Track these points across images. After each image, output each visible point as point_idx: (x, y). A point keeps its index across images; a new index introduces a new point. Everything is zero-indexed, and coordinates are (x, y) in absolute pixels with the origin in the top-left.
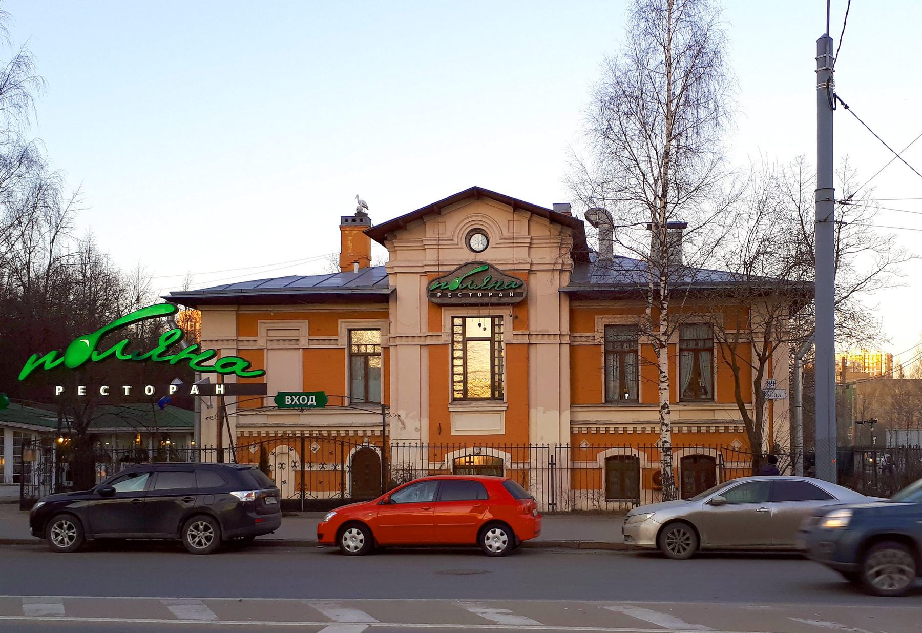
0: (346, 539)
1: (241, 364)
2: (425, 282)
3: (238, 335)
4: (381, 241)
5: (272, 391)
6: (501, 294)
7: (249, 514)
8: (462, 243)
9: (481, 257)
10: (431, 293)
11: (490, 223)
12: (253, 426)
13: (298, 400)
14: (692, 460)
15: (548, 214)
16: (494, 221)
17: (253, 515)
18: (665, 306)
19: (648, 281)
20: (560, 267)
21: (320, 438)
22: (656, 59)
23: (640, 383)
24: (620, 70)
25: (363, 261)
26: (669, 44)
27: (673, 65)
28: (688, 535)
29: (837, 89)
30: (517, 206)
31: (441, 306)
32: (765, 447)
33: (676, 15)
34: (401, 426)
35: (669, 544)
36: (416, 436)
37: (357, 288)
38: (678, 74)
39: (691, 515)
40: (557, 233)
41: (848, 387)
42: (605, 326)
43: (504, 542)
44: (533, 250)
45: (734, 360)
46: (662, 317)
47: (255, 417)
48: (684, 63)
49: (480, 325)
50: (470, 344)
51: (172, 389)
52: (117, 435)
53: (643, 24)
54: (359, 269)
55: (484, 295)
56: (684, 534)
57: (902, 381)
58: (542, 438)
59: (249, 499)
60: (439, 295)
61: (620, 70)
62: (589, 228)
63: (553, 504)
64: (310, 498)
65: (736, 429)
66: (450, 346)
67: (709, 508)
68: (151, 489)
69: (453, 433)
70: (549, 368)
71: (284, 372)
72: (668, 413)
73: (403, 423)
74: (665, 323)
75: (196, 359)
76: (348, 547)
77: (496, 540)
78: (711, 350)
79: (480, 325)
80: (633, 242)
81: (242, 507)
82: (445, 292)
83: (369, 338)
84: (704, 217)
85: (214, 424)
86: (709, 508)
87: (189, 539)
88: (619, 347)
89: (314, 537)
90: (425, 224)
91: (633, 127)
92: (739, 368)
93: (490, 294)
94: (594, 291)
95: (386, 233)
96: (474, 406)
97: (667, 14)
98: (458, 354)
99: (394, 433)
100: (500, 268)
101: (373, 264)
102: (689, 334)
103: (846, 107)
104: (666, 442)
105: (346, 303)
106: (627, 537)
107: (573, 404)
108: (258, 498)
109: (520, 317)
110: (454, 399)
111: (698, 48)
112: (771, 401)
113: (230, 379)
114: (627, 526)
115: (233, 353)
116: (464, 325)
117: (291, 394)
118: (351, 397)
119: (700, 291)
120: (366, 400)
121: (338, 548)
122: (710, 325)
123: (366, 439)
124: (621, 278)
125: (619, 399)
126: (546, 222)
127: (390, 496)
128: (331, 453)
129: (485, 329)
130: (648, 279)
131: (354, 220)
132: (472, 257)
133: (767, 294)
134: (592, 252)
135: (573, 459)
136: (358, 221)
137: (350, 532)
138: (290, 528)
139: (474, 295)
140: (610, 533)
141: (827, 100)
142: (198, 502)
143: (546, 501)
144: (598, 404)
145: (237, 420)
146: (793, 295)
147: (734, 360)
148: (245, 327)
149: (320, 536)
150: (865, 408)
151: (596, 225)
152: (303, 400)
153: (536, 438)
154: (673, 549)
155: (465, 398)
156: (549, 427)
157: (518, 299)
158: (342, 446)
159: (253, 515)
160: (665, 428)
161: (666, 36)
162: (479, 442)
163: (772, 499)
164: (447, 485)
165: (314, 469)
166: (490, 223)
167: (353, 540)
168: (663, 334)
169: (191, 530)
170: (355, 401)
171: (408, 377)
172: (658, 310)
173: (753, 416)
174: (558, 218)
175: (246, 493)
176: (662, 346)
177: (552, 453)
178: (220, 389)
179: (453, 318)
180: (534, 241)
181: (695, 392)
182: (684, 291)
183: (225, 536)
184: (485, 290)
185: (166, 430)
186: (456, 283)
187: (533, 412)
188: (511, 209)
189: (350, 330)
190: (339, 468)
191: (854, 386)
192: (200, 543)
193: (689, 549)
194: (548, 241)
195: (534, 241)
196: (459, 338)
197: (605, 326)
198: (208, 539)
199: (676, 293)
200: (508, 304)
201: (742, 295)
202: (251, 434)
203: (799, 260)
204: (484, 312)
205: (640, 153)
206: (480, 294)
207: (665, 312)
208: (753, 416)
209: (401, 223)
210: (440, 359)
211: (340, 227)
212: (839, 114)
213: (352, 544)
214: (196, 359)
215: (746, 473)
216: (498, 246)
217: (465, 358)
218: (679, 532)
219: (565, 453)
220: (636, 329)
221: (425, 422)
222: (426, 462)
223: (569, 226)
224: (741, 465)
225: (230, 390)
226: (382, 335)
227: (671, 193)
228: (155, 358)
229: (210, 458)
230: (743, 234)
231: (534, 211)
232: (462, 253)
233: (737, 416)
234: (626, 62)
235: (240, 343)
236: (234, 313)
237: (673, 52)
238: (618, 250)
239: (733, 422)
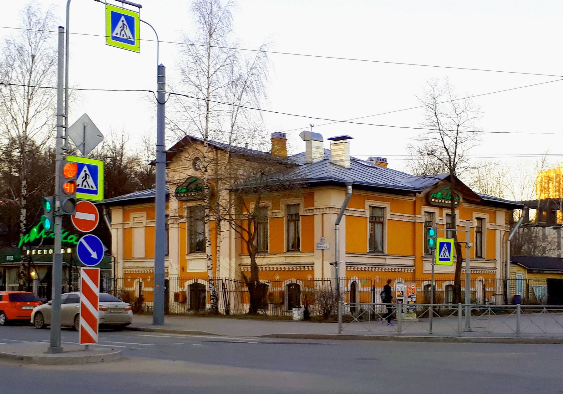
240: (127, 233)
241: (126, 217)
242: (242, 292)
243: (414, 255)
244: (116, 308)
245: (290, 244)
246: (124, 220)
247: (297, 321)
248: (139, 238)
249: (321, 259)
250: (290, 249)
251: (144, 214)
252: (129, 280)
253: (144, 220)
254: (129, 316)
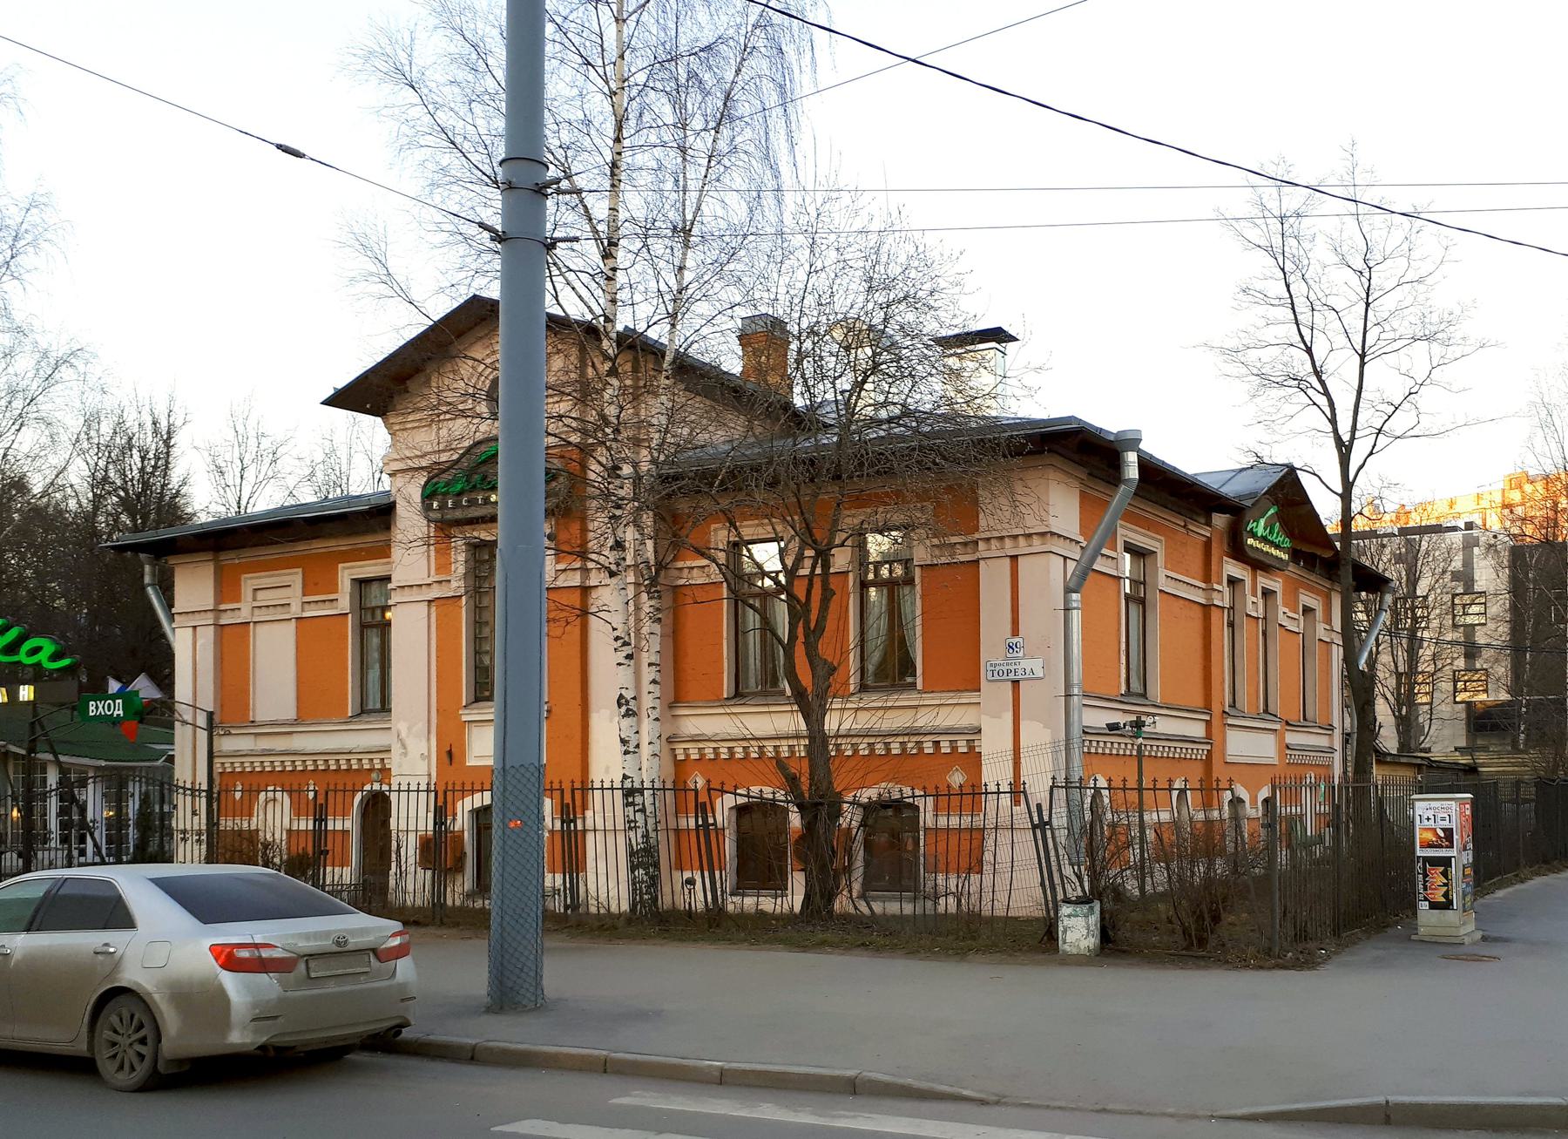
3: (218, 601)
123: (374, 775)
240: (232, 645)
241: (226, 589)
242: (677, 831)
243: (1208, 708)
244: (341, 952)
245: (871, 668)
246: (220, 596)
247: (1079, 960)
248: (275, 659)
249: (1009, 716)
250: (870, 681)
251: (295, 578)
252: (238, 795)
253: (294, 596)
254: (403, 986)
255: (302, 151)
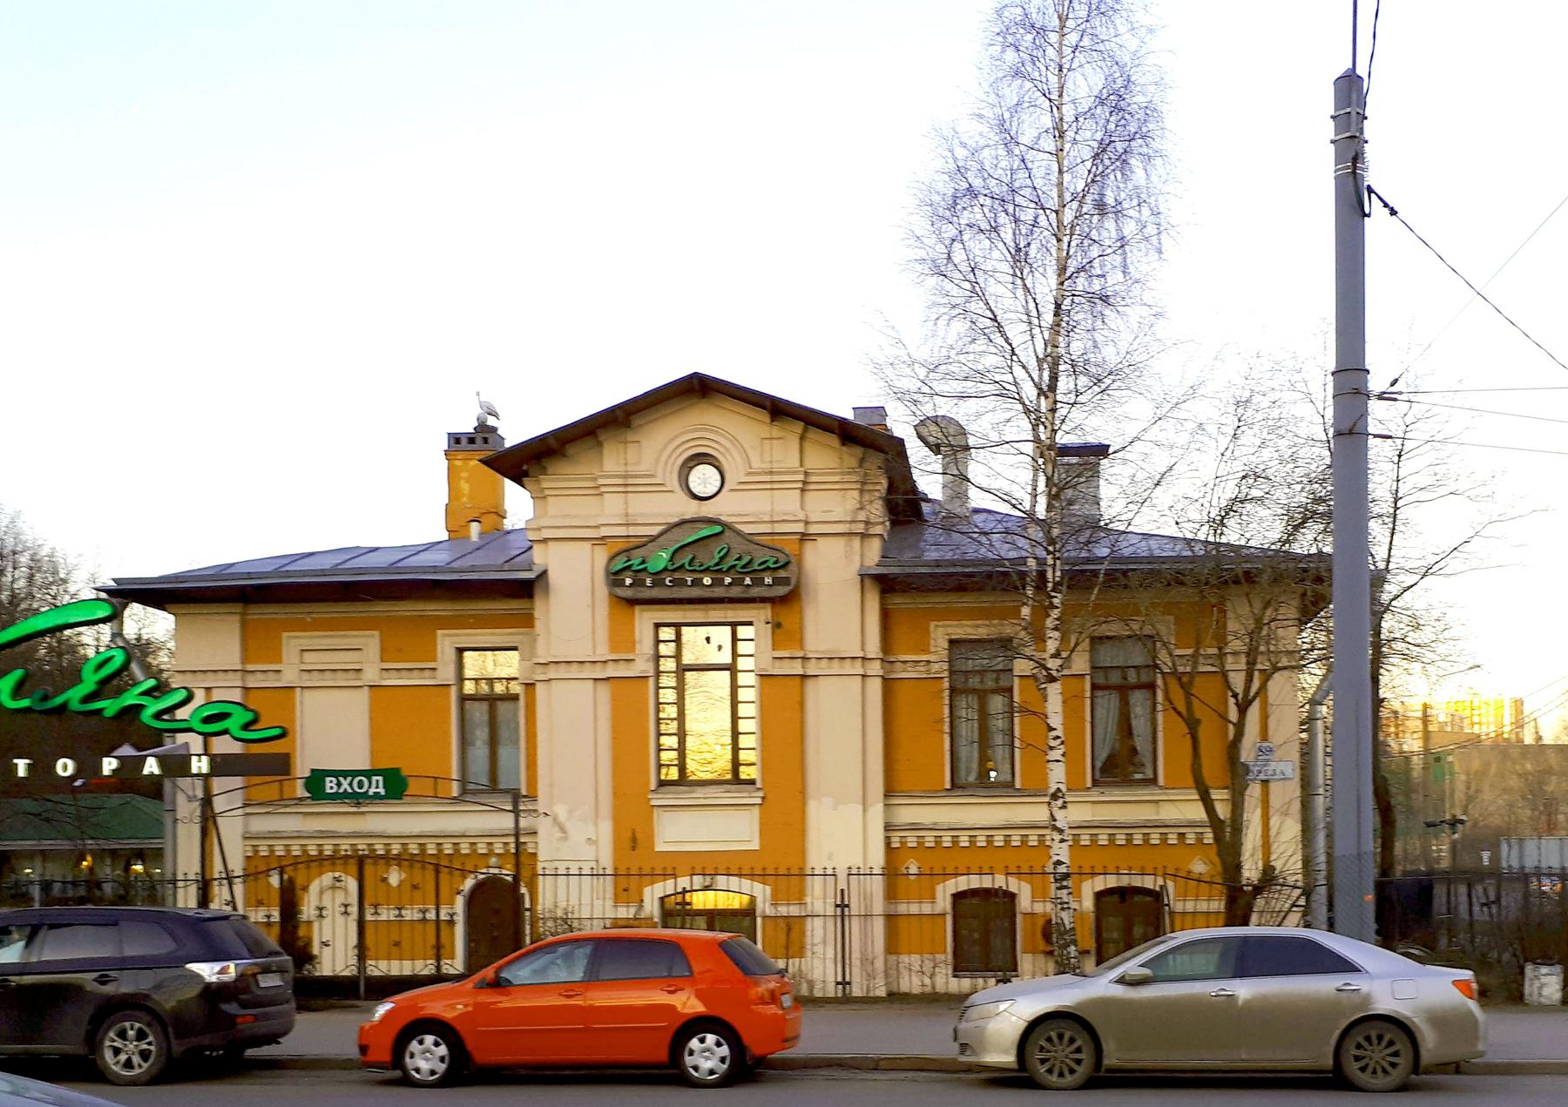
0: (412, 1056)
1: (240, 717)
2: (602, 555)
3: (244, 660)
4: (518, 479)
5: (302, 769)
6: (748, 581)
7: (225, 1007)
8: (673, 482)
9: (708, 510)
10: (614, 578)
11: (728, 445)
12: (276, 835)
13: (351, 784)
14: (1115, 898)
15: (836, 424)
16: (735, 441)
17: (231, 1008)
18: (1056, 601)
19: (1024, 554)
20: (860, 528)
21: (401, 860)
22: (1035, 124)
23: (1017, 752)
24: (963, 145)
25: (490, 520)
26: (1061, 96)
27: (1070, 134)
28: (1078, 1043)
29: (1372, 178)
30: (778, 410)
31: (633, 602)
32: (1251, 871)
33: (1072, 38)
34: (559, 835)
35: (1043, 1061)
36: (588, 853)
37: (473, 569)
38: (1080, 154)
39: (1081, 1005)
40: (853, 462)
41: (1438, 760)
42: (951, 642)
43: (723, 1060)
44: (808, 495)
45: (1189, 706)
46: (1049, 623)
47: (350, 819)
48: (1090, 134)
49: (708, 639)
50: (690, 676)
51: (109, 765)
52: (44, 855)
53: (1011, 56)
54: (482, 534)
55: (717, 582)
56: (1072, 1041)
57: (1540, 748)
58: (830, 857)
59: (225, 978)
60: (628, 581)
61: (963, 145)
62: (916, 452)
63: (845, 983)
64: (377, 973)
65: (1200, 839)
66: (651, 681)
67: (1120, 991)
68: (34, 959)
69: (660, 847)
70: (843, 722)
71: (333, 729)
72: (1064, 807)
73: (563, 830)
74: (1057, 634)
75: (153, 706)
76: (417, 1070)
77: (706, 1055)
78: (1151, 687)
79: (708, 639)
80: (1004, 480)
81: (213, 994)
82: (640, 576)
83: (493, 666)
84: (1132, 430)
85: (196, 830)
86: (1120, 991)
87: (108, 1055)
88: (977, 681)
89: (353, 1052)
90: (600, 444)
91: (997, 260)
92: (1198, 722)
93: (728, 580)
94: (928, 570)
95: (528, 461)
96: (699, 795)
97: (1053, 38)
98: (668, 696)
99: (547, 848)
100: (747, 529)
101: (508, 524)
102: (1108, 657)
103: (1393, 212)
104: (1059, 863)
105: (453, 599)
106: (964, 1047)
107: (889, 792)
108: (241, 977)
109: (785, 624)
110: (662, 784)
111: (1115, 100)
112: (1265, 782)
113: (223, 746)
114: (963, 1026)
115: (236, 696)
116: (678, 640)
117: (336, 774)
118: (463, 781)
119: (1125, 573)
120: (493, 787)
121: (397, 1073)
122: (1149, 640)
123: (493, 861)
124: (971, 551)
125: (970, 781)
126: (834, 441)
127: (500, 968)
128: (415, 887)
129: (720, 648)
130: (1024, 551)
131: (472, 441)
132: (692, 509)
133: (1249, 577)
134: (928, 500)
135: (891, 894)
136: (479, 441)
137: (421, 1042)
138: (318, 1033)
139: (697, 583)
140: (928, 1038)
141: (1354, 199)
142: (125, 985)
143: (831, 979)
144: (932, 793)
145: (246, 825)
146: (1305, 586)
147: (1189, 706)
148: (257, 647)
149: (363, 1049)
150: (1470, 799)
151: (936, 449)
152: (361, 785)
153: (816, 859)
154: (1050, 1071)
155: (683, 780)
156: (845, 835)
157: (781, 591)
158: (437, 872)
159: (231, 1008)
160: (1057, 837)
161: (1053, 79)
162: (711, 866)
163: (1241, 972)
164: (614, 951)
165: (384, 917)
166: (728, 445)
167: (427, 1057)
168: (1053, 656)
169: (111, 1039)
170: (472, 787)
171: (570, 743)
172: (1043, 610)
173: (1223, 811)
174: (863, 439)
175: (217, 966)
176: (1052, 679)
177: (842, 885)
178: (200, 765)
179: (658, 626)
180: (813, 479)
181: (1119, 766)
182: (1095, 573)
183: (177, 1049)
184: (717, 571)
185: (135, 844)
186: (661, 559)
187: (813, 806)
188: (765, 416)
189: (461, 651)
190: (431, 915)
191: (1450, 759)
192: (128, 1064)
193: (1080, 1069)
194: (837, 478)
195: (813, 479)
196: (669, 665)
197: (951, 642)
198: (144, 1055)
199: (1078, 579)
200: (763, 600)
201: (1214, 582)
202: (272, 852)
203: (1308, 516)
204: (716, 613)
205: (1007, 301)
206: (707, 581)
207: (1055, 613)
208: (1223, 811)
209: (552, 441)
210: (636, 711)
211: (446, 453)
212: (1377, 225)
213: (424, 1065)
214: (153, 706)
215: (1212, 921)
216: (743, 487)
217: (680, 704)
218: (1061, 1037)
219: (877, 885)
220: (1005, 645)
221: (605, 830)
222: (609, 903)
223: (880, 449)
224: (1203, 906)
225: (222, 765)
226: (522, 659)
227: (1064, 384)
228: (75, 705)
229: (187, 899)
230: (1207, 464)
231: (811, 421)
232: (657, 496)
233: (1197, 812)
234: (977, 132)
235: (250, 677)
236: (237, 618)
237: (1068, 112)
238: (977, 499)
239: (1191, 825)
255: (1326, 102)
